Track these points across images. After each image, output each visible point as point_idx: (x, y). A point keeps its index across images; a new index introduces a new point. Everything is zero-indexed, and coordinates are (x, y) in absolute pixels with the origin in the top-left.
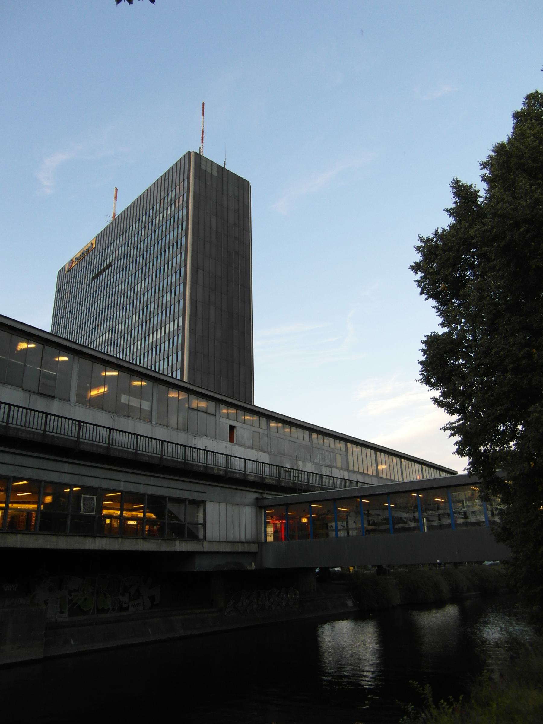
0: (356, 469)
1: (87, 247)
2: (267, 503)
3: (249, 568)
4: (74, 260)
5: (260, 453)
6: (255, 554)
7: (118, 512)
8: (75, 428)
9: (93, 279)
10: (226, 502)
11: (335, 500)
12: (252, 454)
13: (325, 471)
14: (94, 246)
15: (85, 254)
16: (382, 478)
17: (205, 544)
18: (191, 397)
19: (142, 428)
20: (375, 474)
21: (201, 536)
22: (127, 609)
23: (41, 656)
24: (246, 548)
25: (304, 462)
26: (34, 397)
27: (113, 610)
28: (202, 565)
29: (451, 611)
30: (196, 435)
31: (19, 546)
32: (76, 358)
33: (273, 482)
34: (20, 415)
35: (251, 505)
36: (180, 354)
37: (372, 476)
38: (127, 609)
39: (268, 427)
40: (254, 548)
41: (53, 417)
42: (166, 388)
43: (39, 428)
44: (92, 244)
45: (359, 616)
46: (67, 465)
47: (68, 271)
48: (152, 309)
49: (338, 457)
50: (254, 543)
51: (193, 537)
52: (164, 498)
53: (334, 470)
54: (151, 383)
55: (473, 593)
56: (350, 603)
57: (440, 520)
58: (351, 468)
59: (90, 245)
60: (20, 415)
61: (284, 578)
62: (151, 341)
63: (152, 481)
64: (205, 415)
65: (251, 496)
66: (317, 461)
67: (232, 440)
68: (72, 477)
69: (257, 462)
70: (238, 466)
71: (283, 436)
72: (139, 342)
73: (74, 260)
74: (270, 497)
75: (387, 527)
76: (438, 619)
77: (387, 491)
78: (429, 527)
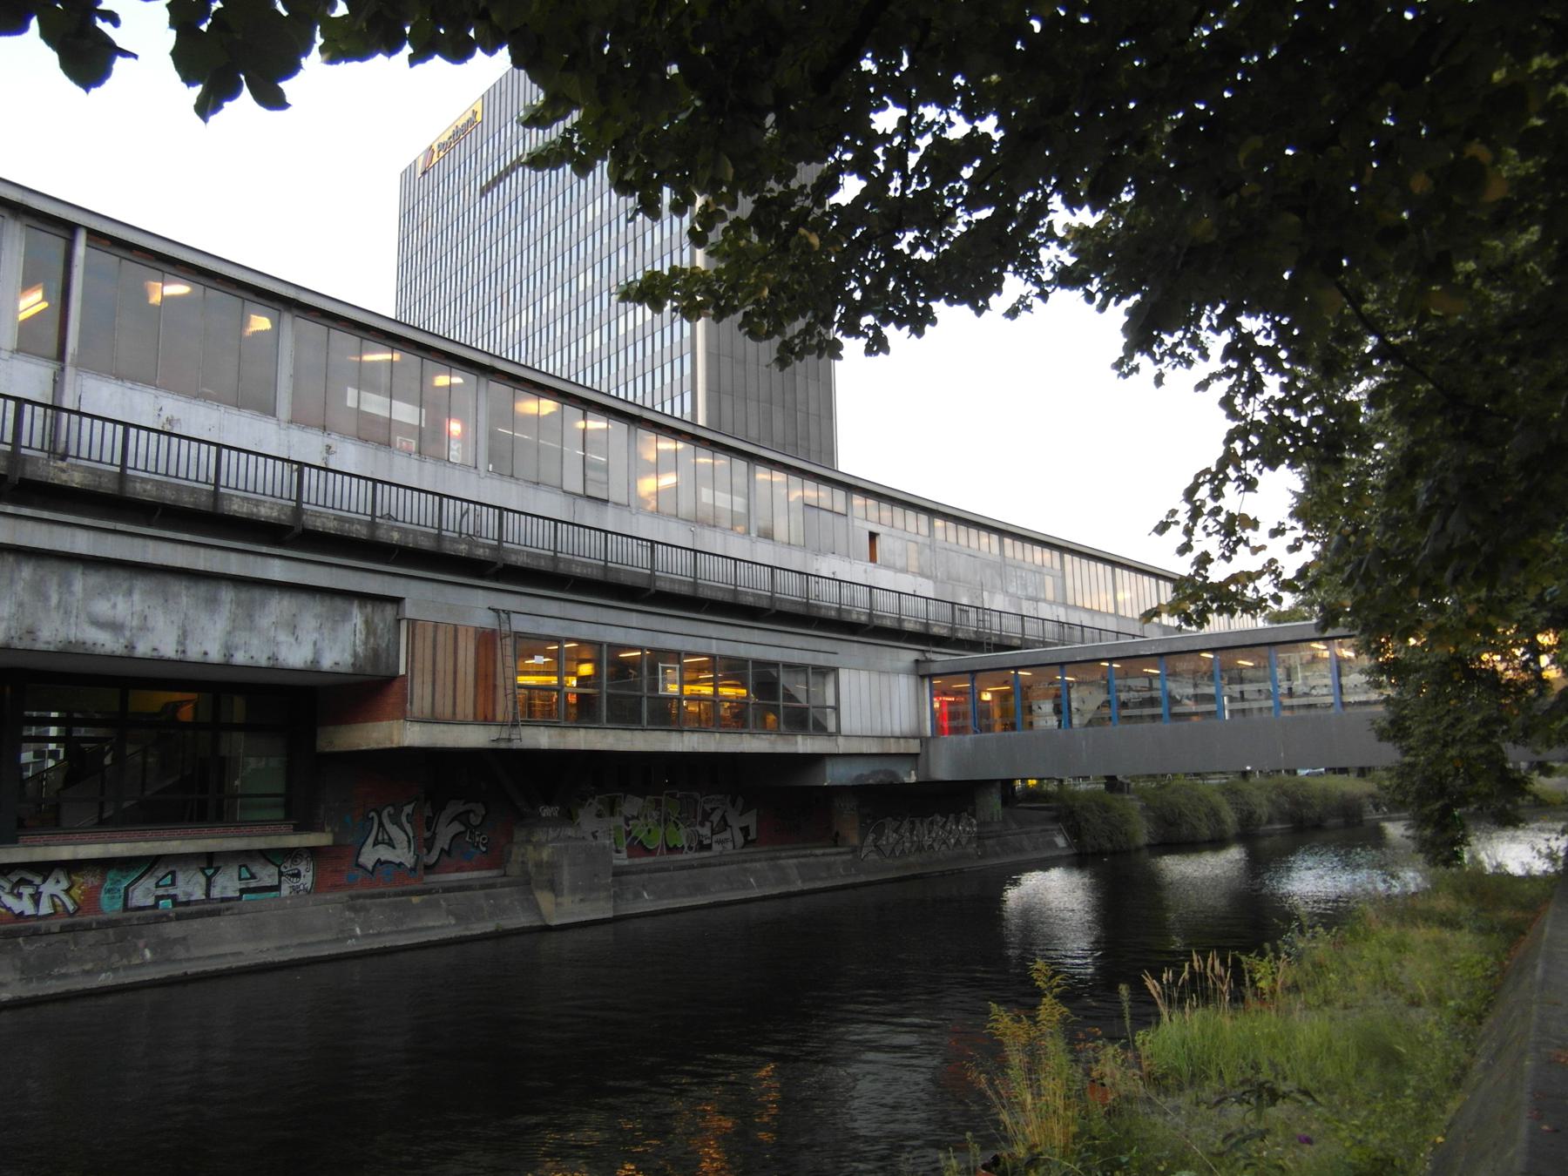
0: (1079, 603)
1: (464, 120)
2: (935, 668)
3: (906, 780)
4: (435, 148)
5: (920, 580)
6: (917, 755)
7: (554, 680)
8: (646, 553)
9: (483, 192)
10: (868, 668)
11: (1062, 664)
12: (906, 583)
13: (1027, 608)
14: (479, 118)
15: (460, 134)
16: (1124, 617)
17: (840, 740)
18: (430, 365)
19: (737, 547)
20: (1111, 610)
21: (832, 727)
22: (709, 847)
23: (610, 914)
24: (903, 747)
25: (992, 593)
26: (581, 503)
27: (690, 848)
28: (835, 775)
29: (1234, 855)
30: (818, 552)
31: (583, 747)
32: (483, 380)
33: (944, 632)
34: (153, 448)
35: (908, 673)
36: (687, 359)
37: (1108, 613)
38: (709, 847)
39: (931, 527)
40: (914, 747)
41: (143, 434)
42: (236, 302)
43: (107, 458)
44: (475, 113)
45: (1077, 860)
46: (634, 615)
47: (424, 173)
48: (622, 262)
49: (1049, 581)
50: (914, 738)
51: (820, 729)
52: (775, 664)
53: (1042, 605)
54: (473, 378)
55: (1278, 826)
56: (1061, 842)
57: (1242, 693)
58: (1070, 601)
59: (469, 115)
60: (153, 448)
61: (954, 797)
62: (622, 331)
63: (756, 636)
64: (830, 515)
65: (908, 656)
66: (1012, 590)
67: (873, 559)
68: (632, 631)
69: (327, 470)
70: (886, 606)
71: (955, 547)
72: (597, 333)
73: (435, 148)
74: (942, 658)
75: (1159, 711)
76: (1203, 873)
77: (1161, 650)
78: (1231, 711)
